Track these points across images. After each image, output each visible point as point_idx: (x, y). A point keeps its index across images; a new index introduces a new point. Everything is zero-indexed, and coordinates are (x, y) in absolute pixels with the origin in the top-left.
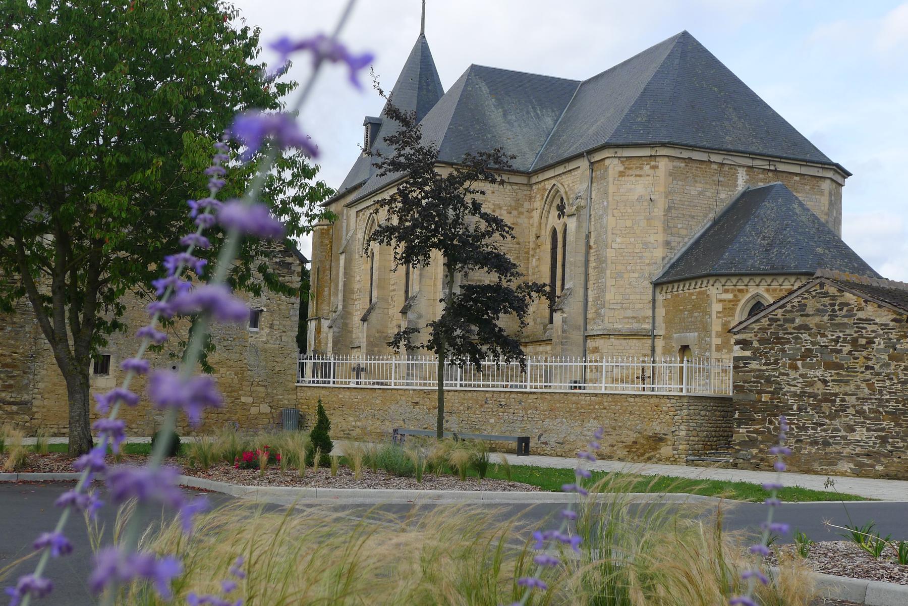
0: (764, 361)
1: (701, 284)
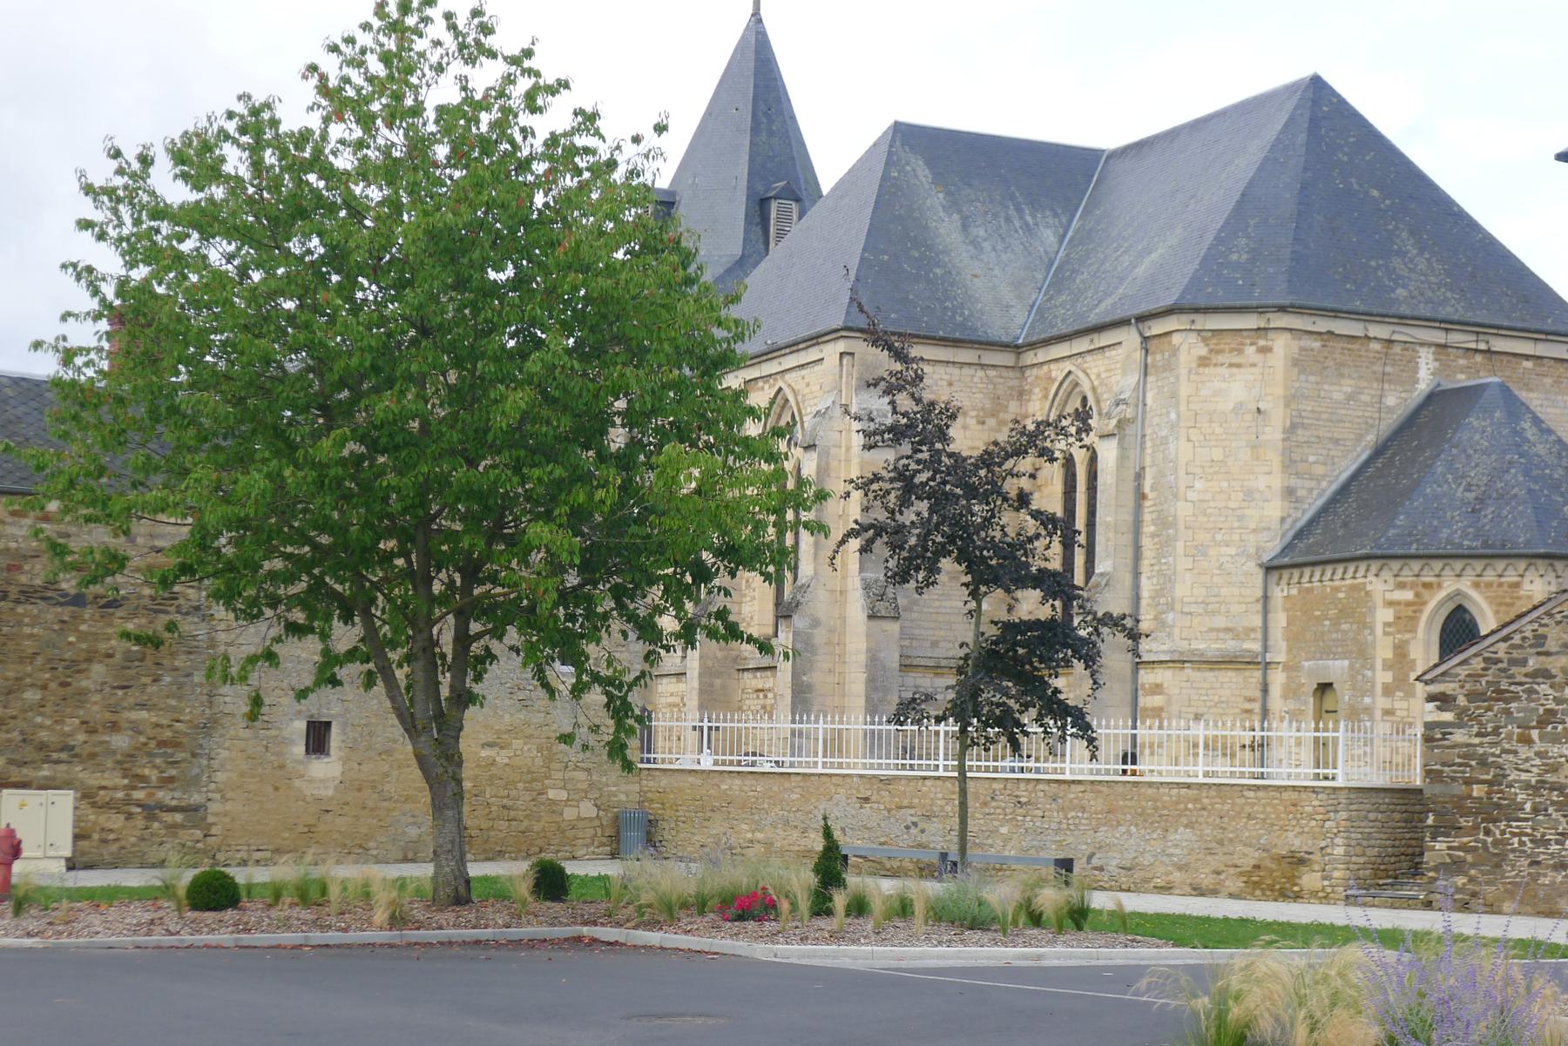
0: (1475, 729)
1: (1355, 572)
